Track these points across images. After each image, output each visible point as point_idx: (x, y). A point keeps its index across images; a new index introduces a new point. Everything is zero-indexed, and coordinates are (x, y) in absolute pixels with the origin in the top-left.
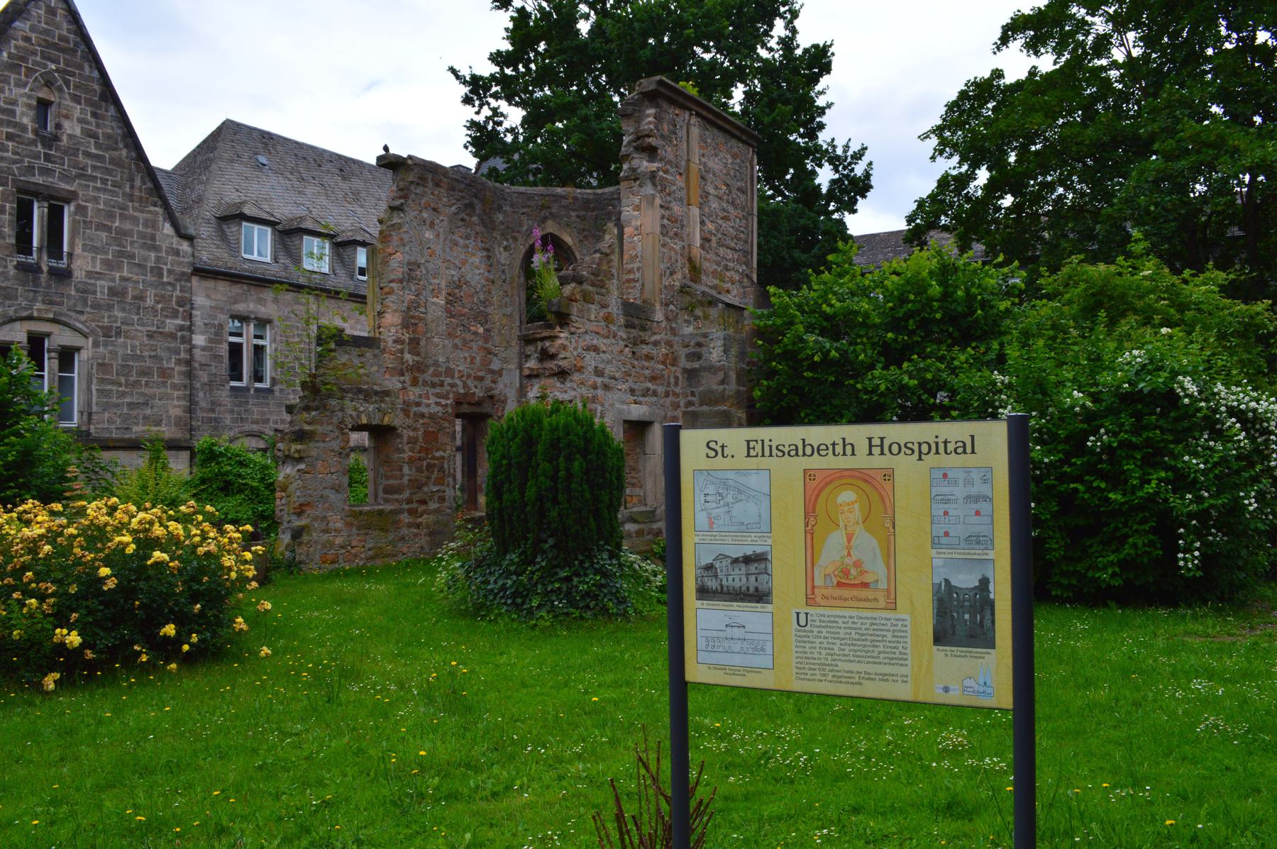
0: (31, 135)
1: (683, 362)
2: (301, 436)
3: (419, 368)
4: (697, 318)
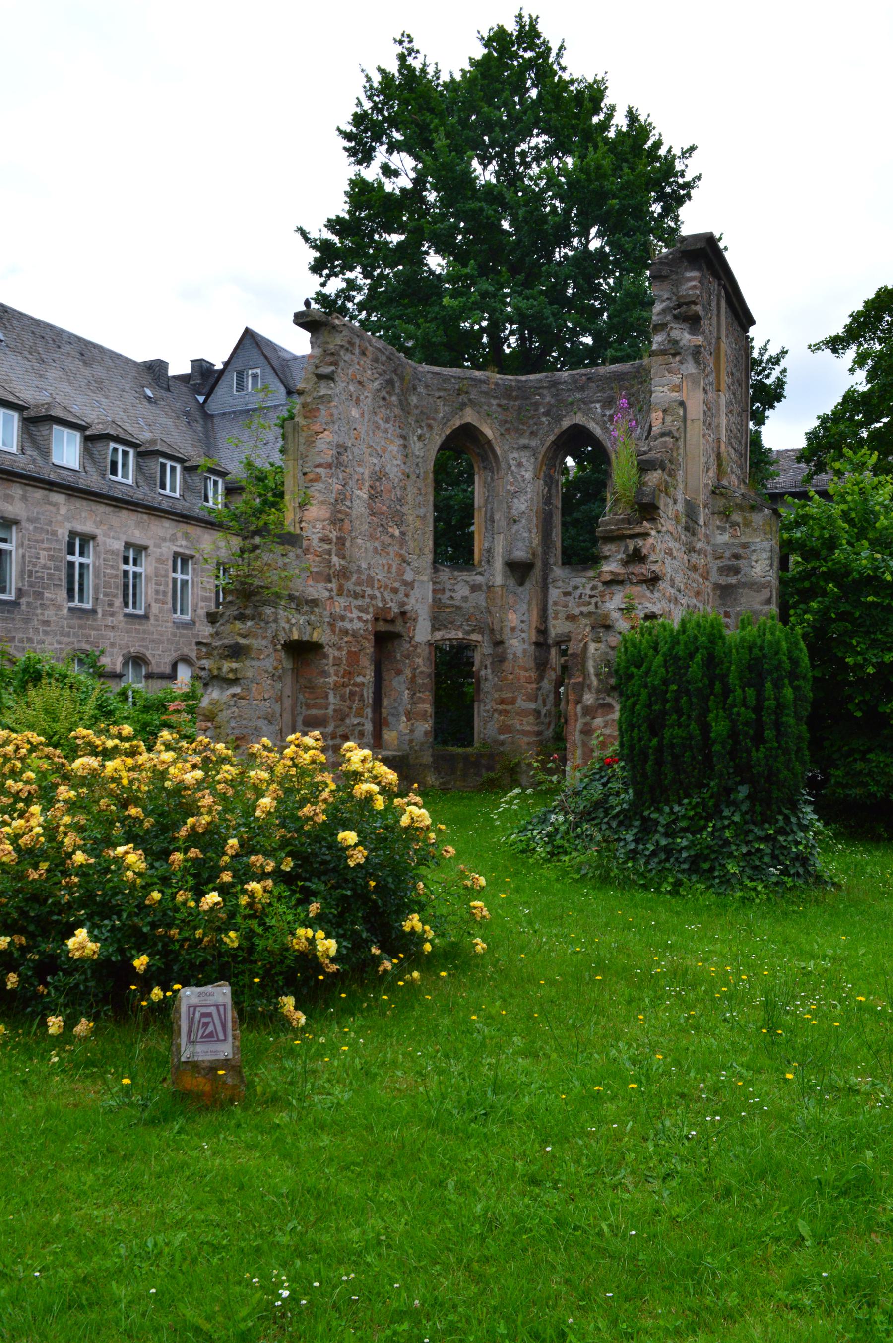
1: (715, 577)
2: (236, 652)
3: (344, 574)
4: (734, 525)
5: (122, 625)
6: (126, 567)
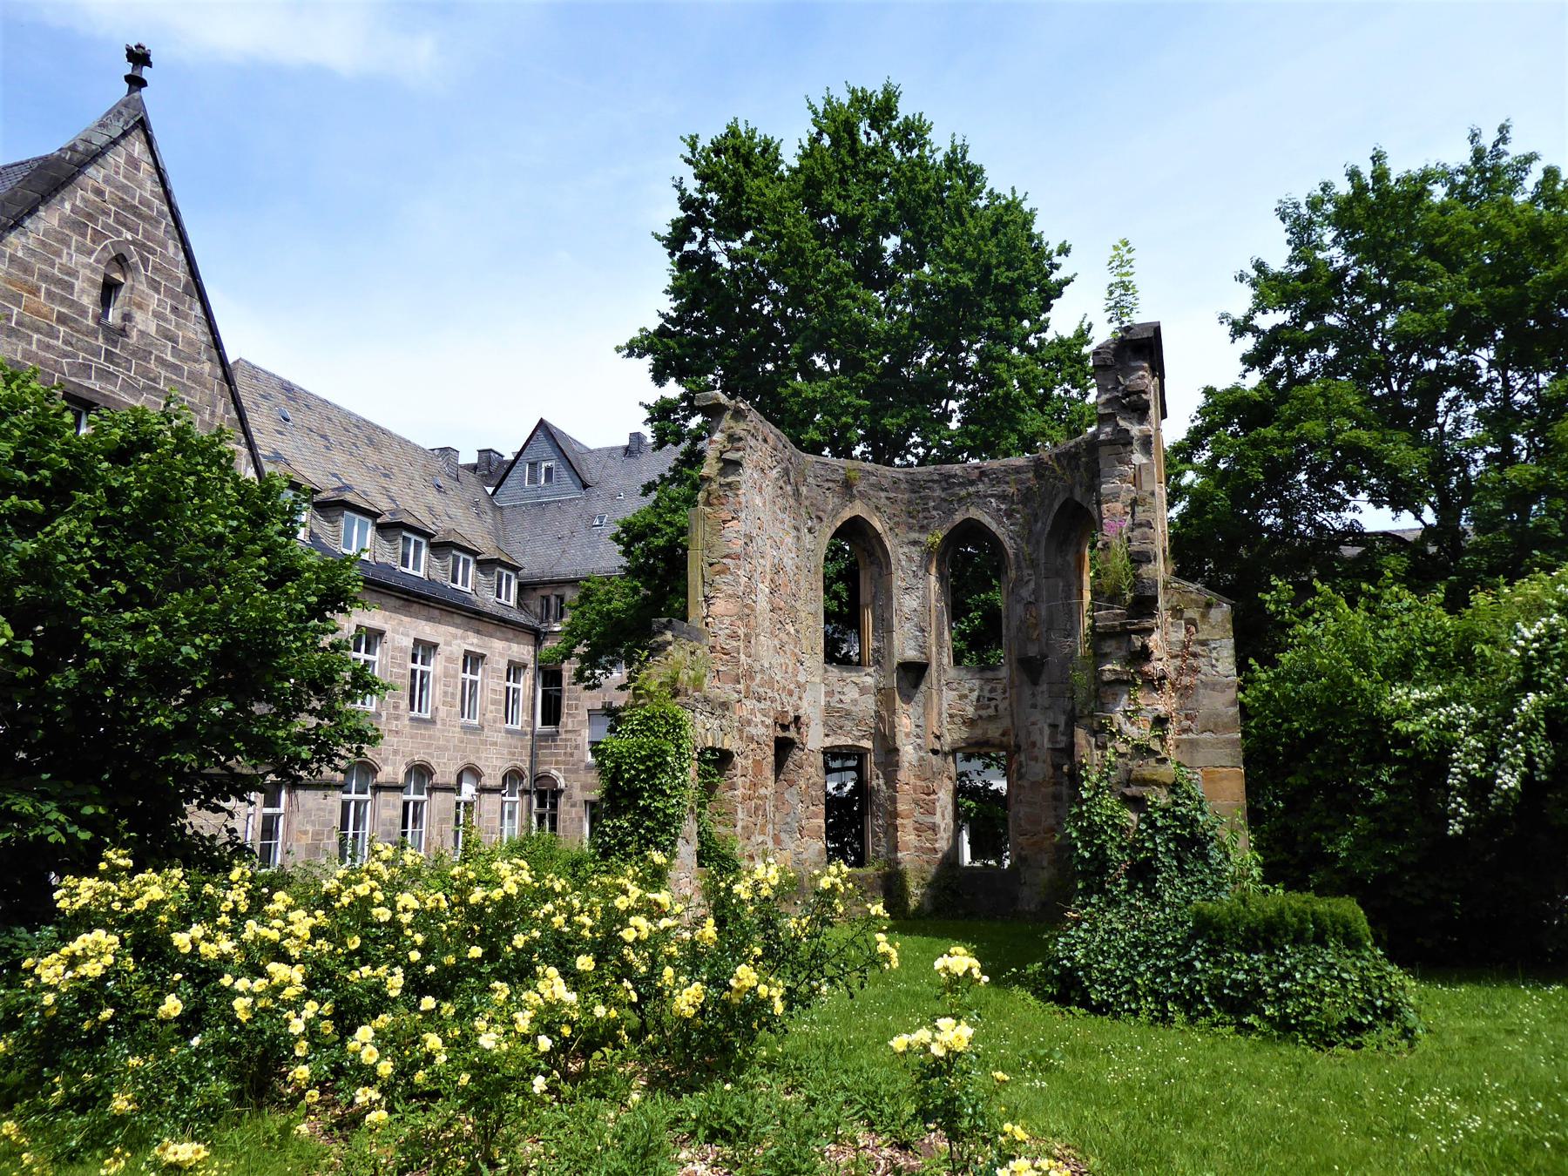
0: (90, 322)
5: (407, 729)
6: (414, 666)
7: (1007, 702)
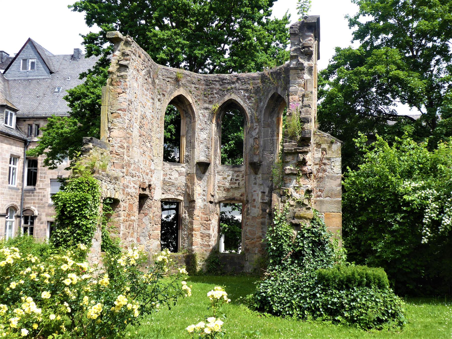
7: (244, 181)
